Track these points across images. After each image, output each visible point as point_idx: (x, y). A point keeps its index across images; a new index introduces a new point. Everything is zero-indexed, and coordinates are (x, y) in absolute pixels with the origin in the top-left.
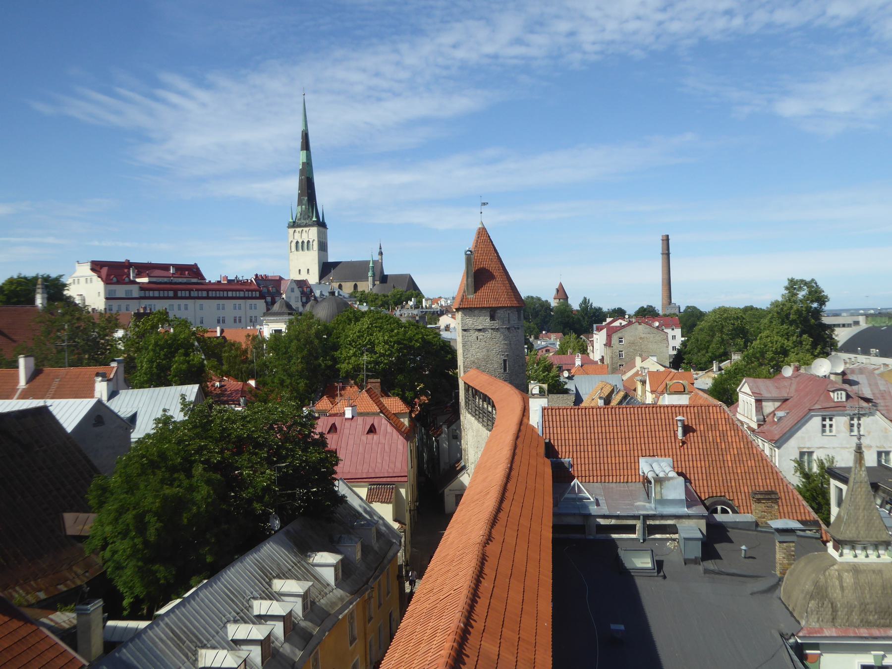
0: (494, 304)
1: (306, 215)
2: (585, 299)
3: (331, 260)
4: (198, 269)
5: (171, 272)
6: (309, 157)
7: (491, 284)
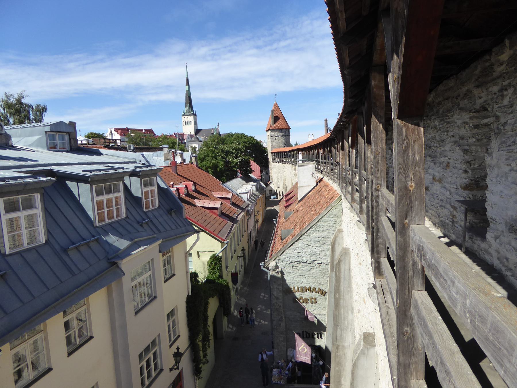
0: (281, 128)
2: (297, 142)
4: (153, 131)
7: (279, 121)
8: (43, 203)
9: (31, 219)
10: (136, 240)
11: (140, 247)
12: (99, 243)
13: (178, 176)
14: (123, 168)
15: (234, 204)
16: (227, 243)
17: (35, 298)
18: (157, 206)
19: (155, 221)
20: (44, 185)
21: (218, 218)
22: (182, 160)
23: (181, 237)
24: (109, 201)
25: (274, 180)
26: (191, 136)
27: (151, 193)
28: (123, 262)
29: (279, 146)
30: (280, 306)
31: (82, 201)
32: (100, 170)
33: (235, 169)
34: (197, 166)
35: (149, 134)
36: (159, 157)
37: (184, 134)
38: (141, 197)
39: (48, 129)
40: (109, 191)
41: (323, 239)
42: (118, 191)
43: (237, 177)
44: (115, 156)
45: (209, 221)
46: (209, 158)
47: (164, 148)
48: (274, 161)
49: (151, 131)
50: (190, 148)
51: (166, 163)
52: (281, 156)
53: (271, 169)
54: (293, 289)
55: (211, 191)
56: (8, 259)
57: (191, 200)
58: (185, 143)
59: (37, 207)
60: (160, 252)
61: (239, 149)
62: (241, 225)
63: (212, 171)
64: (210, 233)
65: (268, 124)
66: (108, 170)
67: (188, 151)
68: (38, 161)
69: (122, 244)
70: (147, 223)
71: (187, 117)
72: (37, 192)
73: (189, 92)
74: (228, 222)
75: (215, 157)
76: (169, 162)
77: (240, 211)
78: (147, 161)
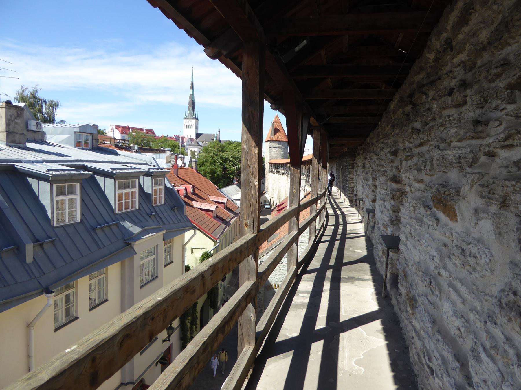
1: (190, 115)
3: (199, 133)
4: (153, 131)
5: (144, 131)
6: (193, 92)
8: (81, 191)
9: (70, 201)
10: (146, 228)
11: (149, 234)
12: (118, 227)
13: (179, 179)
14: (139, 169)
15: (228, 209)
16: (219, 242)
17: (73, 261)
18: (163, 202)
19: (161, 215)
20: (83, 177)
21: (213, 219)
22: (183, 164)
23: (181, 230)
24: (127, 194)
25: (269, 190)
26: (192, 140)
27: (132, 195)
28: (136, 244)
29: (277, 158)
30: (261, 300)
31: (107, 192)
32: (122, 169)
33: (232, 176)
34: (196, 170)
35: (149, 134)
36: (161, 159)
37: (184, 137)
38: (151, 194)
39: (77, 130)
40: (128, 187)
41: (303, 243)
42: (135, 187)
43: (233, 184)
44: (130, 157)
45: (204, 221)
46: (208, 164)
47: (167, 151)
48: (271, 171)
49: (152, 132)
50: (189, 152)
51: (167, 165)
52: (277, 167)
53: (267, 179)
54: (273, 286)
55: (208, 195)
56: (55, 229)
57: (189, 202)
58: (184, 146)
59: (77, 193)
60: (164, 240)
61: (238, 157)
62: (233, 227)
63: (210, 176)
64: (204, 232)
65: (268, 135)
66: (128, 169)
67: (187, 155)
68: (71, 157)
69: (136, 230)
70: (154, 215)
71: (188, 120)
72: (78, 182)
73: (192, 96)
74: (222, 224)
75: (214, 163)
76: (170, 165)
77: (233, 215)
78: (157, 164)
